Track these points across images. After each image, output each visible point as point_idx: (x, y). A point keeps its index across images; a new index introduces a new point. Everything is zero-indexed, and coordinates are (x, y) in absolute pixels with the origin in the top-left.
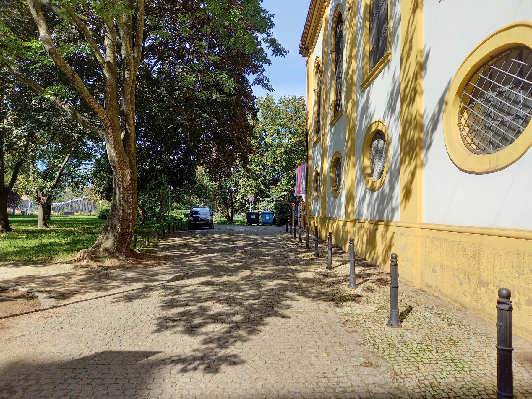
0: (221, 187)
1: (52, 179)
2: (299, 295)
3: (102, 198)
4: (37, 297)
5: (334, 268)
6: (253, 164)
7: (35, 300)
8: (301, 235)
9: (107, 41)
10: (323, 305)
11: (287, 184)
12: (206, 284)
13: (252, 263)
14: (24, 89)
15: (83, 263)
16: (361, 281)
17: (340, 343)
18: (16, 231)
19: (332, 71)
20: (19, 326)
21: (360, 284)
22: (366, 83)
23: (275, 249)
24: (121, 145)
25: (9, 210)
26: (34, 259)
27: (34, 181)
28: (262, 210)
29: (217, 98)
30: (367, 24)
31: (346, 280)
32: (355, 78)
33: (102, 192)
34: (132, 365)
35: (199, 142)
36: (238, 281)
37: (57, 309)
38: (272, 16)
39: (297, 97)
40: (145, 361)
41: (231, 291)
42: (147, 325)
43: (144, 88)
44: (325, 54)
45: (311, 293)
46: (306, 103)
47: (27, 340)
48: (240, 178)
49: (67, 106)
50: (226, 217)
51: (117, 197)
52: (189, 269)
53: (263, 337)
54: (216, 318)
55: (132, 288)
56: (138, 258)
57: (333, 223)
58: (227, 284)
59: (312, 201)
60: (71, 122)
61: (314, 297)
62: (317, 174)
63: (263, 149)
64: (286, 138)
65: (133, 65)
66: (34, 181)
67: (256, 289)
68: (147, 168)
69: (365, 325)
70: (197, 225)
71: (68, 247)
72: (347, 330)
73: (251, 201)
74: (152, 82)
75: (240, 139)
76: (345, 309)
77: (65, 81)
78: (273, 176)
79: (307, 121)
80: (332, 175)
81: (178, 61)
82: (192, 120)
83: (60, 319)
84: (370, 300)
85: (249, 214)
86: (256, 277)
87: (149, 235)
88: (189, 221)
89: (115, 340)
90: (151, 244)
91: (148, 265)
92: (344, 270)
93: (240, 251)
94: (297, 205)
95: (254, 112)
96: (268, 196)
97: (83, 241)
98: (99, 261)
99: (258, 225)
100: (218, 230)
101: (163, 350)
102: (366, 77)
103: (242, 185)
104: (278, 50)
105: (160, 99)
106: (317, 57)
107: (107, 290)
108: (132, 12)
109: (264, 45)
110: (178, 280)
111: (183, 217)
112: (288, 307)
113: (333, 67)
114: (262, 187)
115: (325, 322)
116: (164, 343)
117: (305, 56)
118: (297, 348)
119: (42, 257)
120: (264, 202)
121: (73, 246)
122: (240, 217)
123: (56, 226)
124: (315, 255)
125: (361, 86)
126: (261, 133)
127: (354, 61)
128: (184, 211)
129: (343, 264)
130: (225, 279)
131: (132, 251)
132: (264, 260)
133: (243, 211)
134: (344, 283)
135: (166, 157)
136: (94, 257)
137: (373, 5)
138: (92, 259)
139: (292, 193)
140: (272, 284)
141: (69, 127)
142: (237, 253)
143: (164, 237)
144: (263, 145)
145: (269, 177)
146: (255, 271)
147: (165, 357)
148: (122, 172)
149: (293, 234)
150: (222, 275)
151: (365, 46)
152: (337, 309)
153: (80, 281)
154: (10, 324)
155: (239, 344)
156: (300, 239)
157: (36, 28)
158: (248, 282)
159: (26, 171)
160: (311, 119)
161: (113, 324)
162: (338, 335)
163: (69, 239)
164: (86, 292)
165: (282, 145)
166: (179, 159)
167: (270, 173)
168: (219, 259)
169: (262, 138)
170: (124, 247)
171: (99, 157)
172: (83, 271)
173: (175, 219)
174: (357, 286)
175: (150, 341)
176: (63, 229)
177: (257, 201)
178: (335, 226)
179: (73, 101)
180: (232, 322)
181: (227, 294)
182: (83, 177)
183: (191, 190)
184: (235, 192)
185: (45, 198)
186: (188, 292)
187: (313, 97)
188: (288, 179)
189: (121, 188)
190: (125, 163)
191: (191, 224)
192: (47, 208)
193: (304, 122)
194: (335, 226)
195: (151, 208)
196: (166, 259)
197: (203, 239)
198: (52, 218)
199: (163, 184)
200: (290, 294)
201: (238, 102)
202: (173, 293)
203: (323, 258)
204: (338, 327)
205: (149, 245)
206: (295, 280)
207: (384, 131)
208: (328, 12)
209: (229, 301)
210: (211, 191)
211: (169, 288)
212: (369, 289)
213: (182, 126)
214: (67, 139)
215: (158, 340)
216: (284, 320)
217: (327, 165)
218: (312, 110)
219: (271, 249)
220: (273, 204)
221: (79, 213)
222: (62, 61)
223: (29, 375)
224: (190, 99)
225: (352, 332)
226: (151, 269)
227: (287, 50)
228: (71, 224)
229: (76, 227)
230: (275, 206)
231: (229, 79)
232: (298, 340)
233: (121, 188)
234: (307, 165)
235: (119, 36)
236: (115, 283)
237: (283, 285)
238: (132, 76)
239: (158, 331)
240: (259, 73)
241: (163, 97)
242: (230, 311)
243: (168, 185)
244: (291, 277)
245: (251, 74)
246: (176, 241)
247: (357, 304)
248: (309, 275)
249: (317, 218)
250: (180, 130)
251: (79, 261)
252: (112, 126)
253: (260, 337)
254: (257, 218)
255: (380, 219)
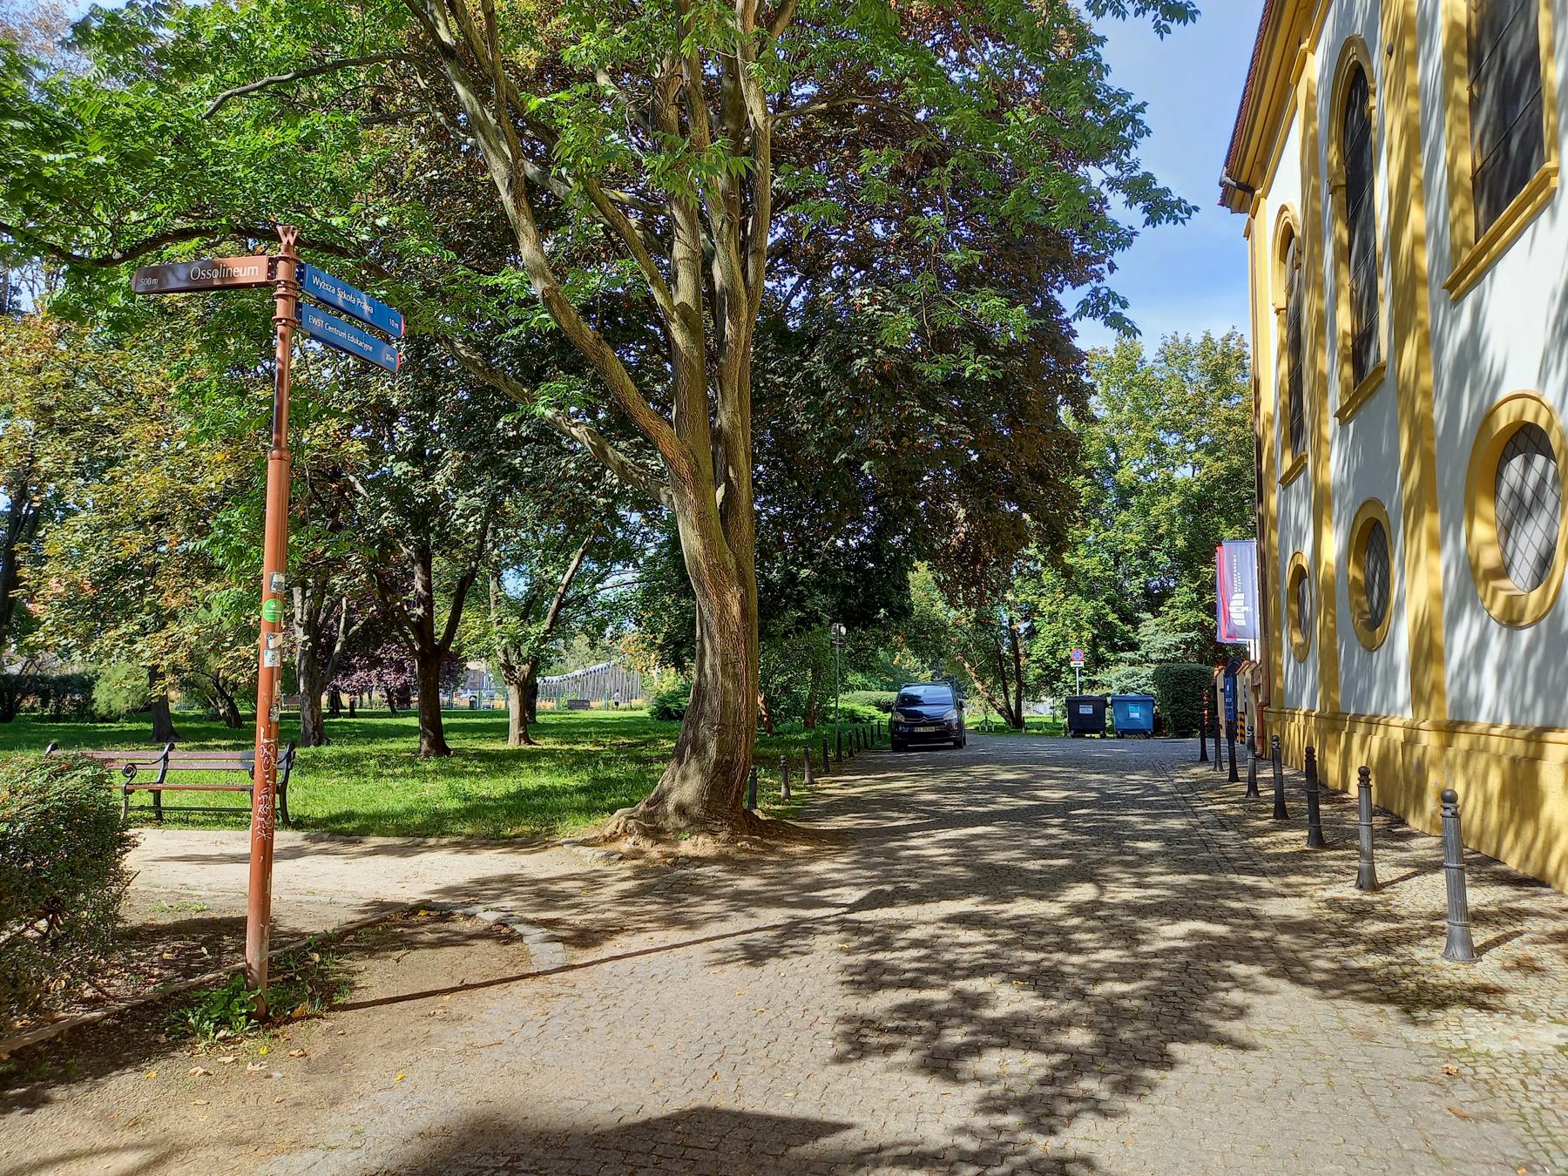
0: (983, 622)
1: (540, 616)
2: (1269, 974)
3: (663, 663)
4: (520, 937)
5: (1383, 885)
6: (1082, 551)
7: (517, 945)
8: (1253, 772)
9: (679, 251)
10: (1356, 1013)
11: (1191, 605)
12: (964, 920)
13: (1099, 861)
14: (479, 393)
15: (625, 845)
16: (1492, 935)
17: (1434, 1153)
18: (460, 753)
19: (1338, 241)
20: (484, 1016)
21: (1487, 947)
22: (1467, 274)
23: (1167, 816)
24: (716, 523)
25: (444, 699)
26: (508, 832)
27: (500, 623)
28: (1115, 690)
29: (976, 372)
30: (1461, 88)
31: (1432, 932)
32: (1425, 260)
33: (661, 648)
34: (776, 1157)
35: (918, 497)
36: (1061, 918)
37: (569, 975)
38: (1141, 108)
39: (1217, 337)
40: (808, 1149)
41: (1041, 949)
42: (805, 1037)
43: (766, 360)
44: (1310, 195)
45: (1309, 969)
46: (1249, 351)
47: (505, 1059)
48: (1041, 595)
49: (584, 428)
50: (1000, 712)
51: (707, 665)
52: (910, 873)
53: (1159, 1108)
54: (1010, 1033)
55: (755, 923)
56: (763, 837)
57: (1368, 733)
58: (1026, 925)
59: (1286, 662)
60: (589, 468)
61: (1321, 985)
62: (1300, 574)
63: (1110, 501)
64: (1184, 463)
65: (744, 307)
66: (500, 623)
67: (1120, 948)
68: (775, 575)
69: (1528, 1099)
70: (918, 736)
71: (583, 798)
72: (1457, 1107)
73: (1077, 664)
74: (787, 341)
75: (1040, 478)
76: (1443, 1035)
77: (575, 366)
78: (1147, 582)
79: (1258, 406)
80: (1353, 571)
81: (858, 276)
82: (897, 436)
83: (581, 1004)
84: (1535, 1009)
85: (1072, 705)
86: (1116, 906)
87: (788, 768)
88: (894, 724)
89: (723, 1075)
90: (793, 793)
91: (793, 857)
92: (1428, 893)
93: (1056, 821)
94: (1231, 673)
95: (1078, 396)
96: (1134, 647)
97: (620, 782)
98: (663, 841)
99: (1103, 737)
100: (981, 751)
101: (856, 1119)
102: (1466, 255)
103: (1044, 610)
104: (1161, 207)
105: (812, 387)
106: (1283, 209)
107: (691, 925)
108: (740, 164)
109: (1116, 200)
110: (881, 905)
111: (873, 711)
112: (1240, 1012)
113: (1341, 230)
114: (1112, 617)
115: (1372, 1074)
116: (858, 1098)
117: (1240, 208)
118: (1281, 1157)
119: (526, 829)
120: (1121, 666)
121: (596, 799)
122: (1042, 710)
123: (550, 740)
124: (1310, 840)
125: (1451, 286)
126: (1101, 456)
127: (1416, 198)
128: (877, 695)
129: (1415, 874)
130: (1023, 907)
131: (748, 814)
132: (1135, 851)
133: (1053, 692)
134: (1427, 942)
135: (826, 545)
136: (655, 833)
137: (1481, 25)
138: (646, 834)
139: (1209, 633)
140: (1172, 933)
141: (583, 480)
142: (1046, 826)
143: (828, 772)
144: (1111, 491)
145: (1134, 586)
146: (1111, 887)
147: (865, 1145)
148: (721, 595)
149: (1227, 767)
150: (1016, 895)
151: (1457, 155)
152: (1410, 1032)
153: (625, 897)
154: (464, 1011)
155: (1087, 1122)
156: (1253, 786)
157: (512, 237)
158: (1092, 923)
159: (482, 597)
160: (1270, 401)
161: (714, 1027)
162: (1421, 1124)
163: (582, 778)
164: (639, 930)
165: (1173, 487)
166: (862, 545)
167: (1137, 574)
168: (996, 844)
169: (1107, 468)
170: (726, 804)
171: (651, 553)
172: (626, 869)
173: (853, 717)
174: (1479, 952)
175: (819, 1089)
176: (566, 747)
177: (1098, 662)
178: (1375, 742)
179: (592, 413)
180: (1058, 1049)
181: (1031, 956)
182: (613, 607)
183: (897, 633)
184: (1028, 637)
185: (525, 667)
186: (916, 944)
187: (1273, 333)
188: (1197, 590)
189: (717, 639)
190: (727, 571)
191: (901, 734)
192: (529, 693)
193: (1247, 410)
194: (1375, 742)
195: (786, 689)
196: (841, 839)
197: (940, 781)
198: (539, 719)
199: (819, 620)
200: (1240, 969)
201: (1033, 372)
202: (870, 944)
203: (1340, 853)
204: (1422, 1096)
205: (788, 796)
206: (1250, 922)
207: (1542, 423)
208: (1316, 67)
209: (1043, 980)
210: (953, 635)
211: (858, 929)
212: (1527, 966)
213: (872, 454)
214: (577, 514)
215: (839, 1087)
216: (1224, 1055)
217: (1333, 544)
218: (1271, 371)
219: (1156, 817)
220: (1150, 672)
221: (602, 703)
222: (574, 316)
223: (518, 1158)
224: (898, 377)
225: (1477, 1120)
226: (801, 868)
227: (1191, 203)
228: (586, 734)
229: (597, 743)
230: (1155, 677)
231: (1013, 305)
232: (1283, 1130)
233: (717, 639)
234: (1265, 546)
235: (709, 231)
236: (712, 907)
237: (1210, 938)
238: (743, 335)
239: (840, 1059)
240: (1094, 282)
241: (819, 380)
242: (1044, 1013)
243: (832, 622)
244: (1235, 913)
245: (1068, 288)
246: (861, 786)
247: (1483, 1016)
248: (1296, 908)
249: (1307, 715)
250: (865, 466)
251: (614, 840)
252: (692, 474)
253: (1149, 1109)
254: (1099, 714)
255: (1549, 723)
